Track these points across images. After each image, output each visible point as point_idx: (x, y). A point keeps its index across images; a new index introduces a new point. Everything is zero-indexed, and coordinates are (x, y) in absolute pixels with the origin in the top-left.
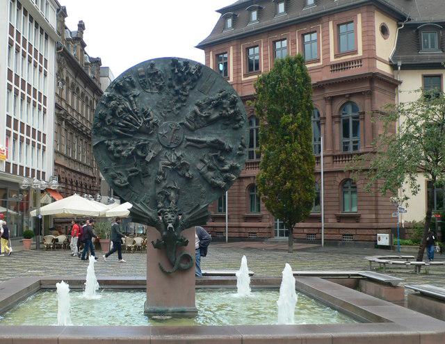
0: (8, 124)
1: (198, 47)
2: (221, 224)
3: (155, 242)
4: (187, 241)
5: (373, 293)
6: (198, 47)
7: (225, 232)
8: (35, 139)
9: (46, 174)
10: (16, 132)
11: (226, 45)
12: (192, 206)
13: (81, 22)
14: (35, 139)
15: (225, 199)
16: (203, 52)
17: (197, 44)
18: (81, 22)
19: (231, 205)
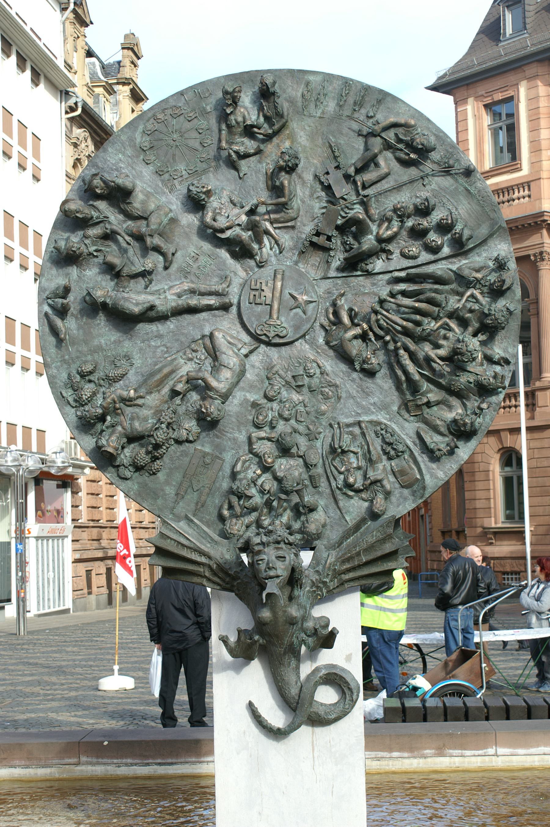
0: (10, 339)
1: (435, 88)
2: (120, 652)
3: (233, 639)
4: (332, 635)
5: (502, 434)
6: (435, 88)
7: (526, 571)
8: (28, 349)
9: (48, 437)
10: (26, 354)
11: (511, 78)
12: (189, 486)
13: (130, 36)
14: (28, 349)
15: (521, 483)
16: (449, 99)
17: (431, 82)
18: (130, 36)
19: (538, 500)
